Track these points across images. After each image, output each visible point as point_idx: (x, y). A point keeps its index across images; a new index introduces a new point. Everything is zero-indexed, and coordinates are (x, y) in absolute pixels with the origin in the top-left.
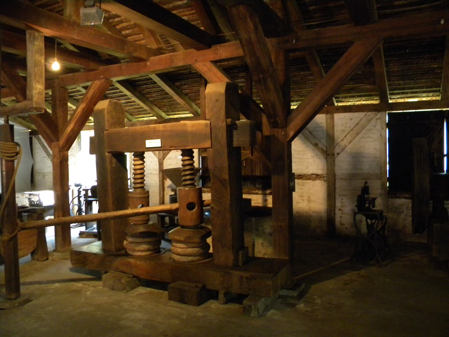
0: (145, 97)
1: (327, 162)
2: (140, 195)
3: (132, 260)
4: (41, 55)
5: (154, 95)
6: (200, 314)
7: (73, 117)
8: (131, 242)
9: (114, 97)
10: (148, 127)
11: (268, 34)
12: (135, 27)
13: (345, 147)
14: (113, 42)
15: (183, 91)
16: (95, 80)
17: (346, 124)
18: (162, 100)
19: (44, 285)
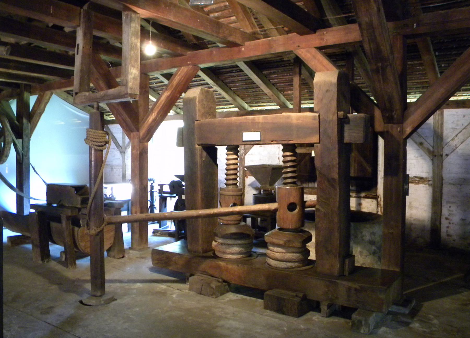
1: (433, 163)
2: (233, 193)
3: (222, 264)
4: (137, 38)
5: (237, 84)
6: (302, 327)
7: (155, 106)
8: (222, 244)
9: (193, 85)
10: (246, 118)
11: (389, 19)
12: (225, 10)
13: (456, 147)
14: (209, 24)
15: (271, 81)
16: (181, 66)
17: (458, 121)
18: (247, 90)
19: (126, 284)
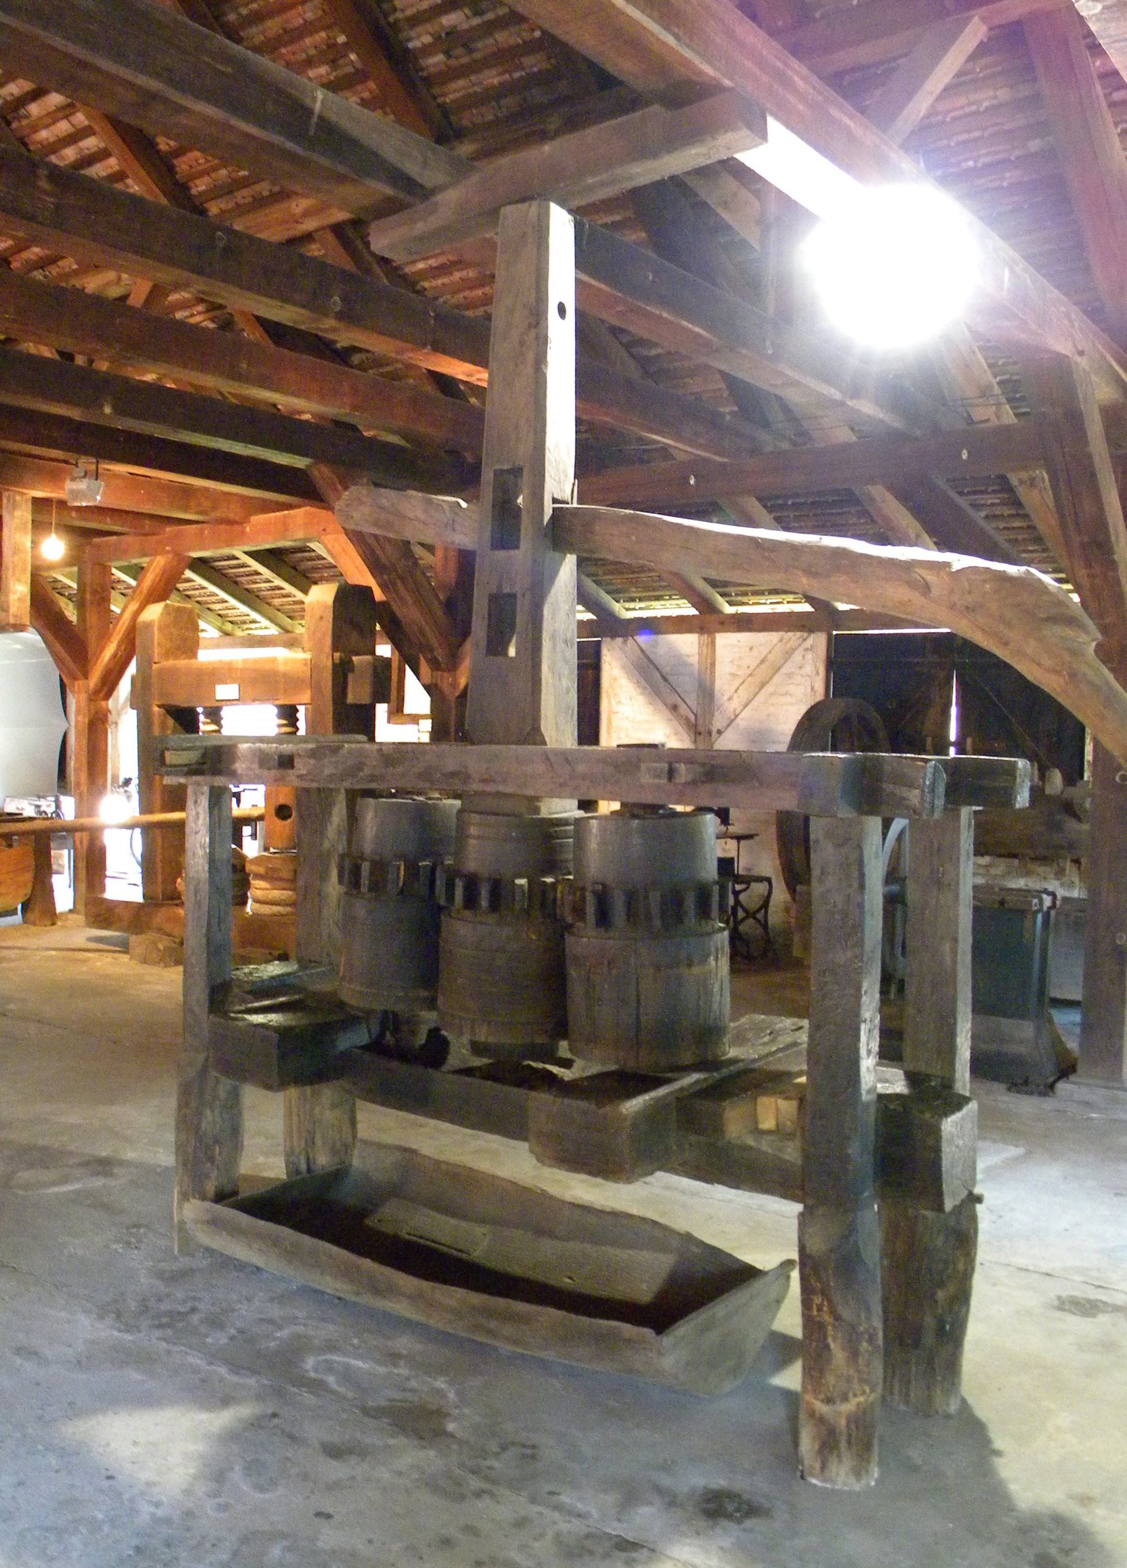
0: (307, 578)
17: (740, 658)
